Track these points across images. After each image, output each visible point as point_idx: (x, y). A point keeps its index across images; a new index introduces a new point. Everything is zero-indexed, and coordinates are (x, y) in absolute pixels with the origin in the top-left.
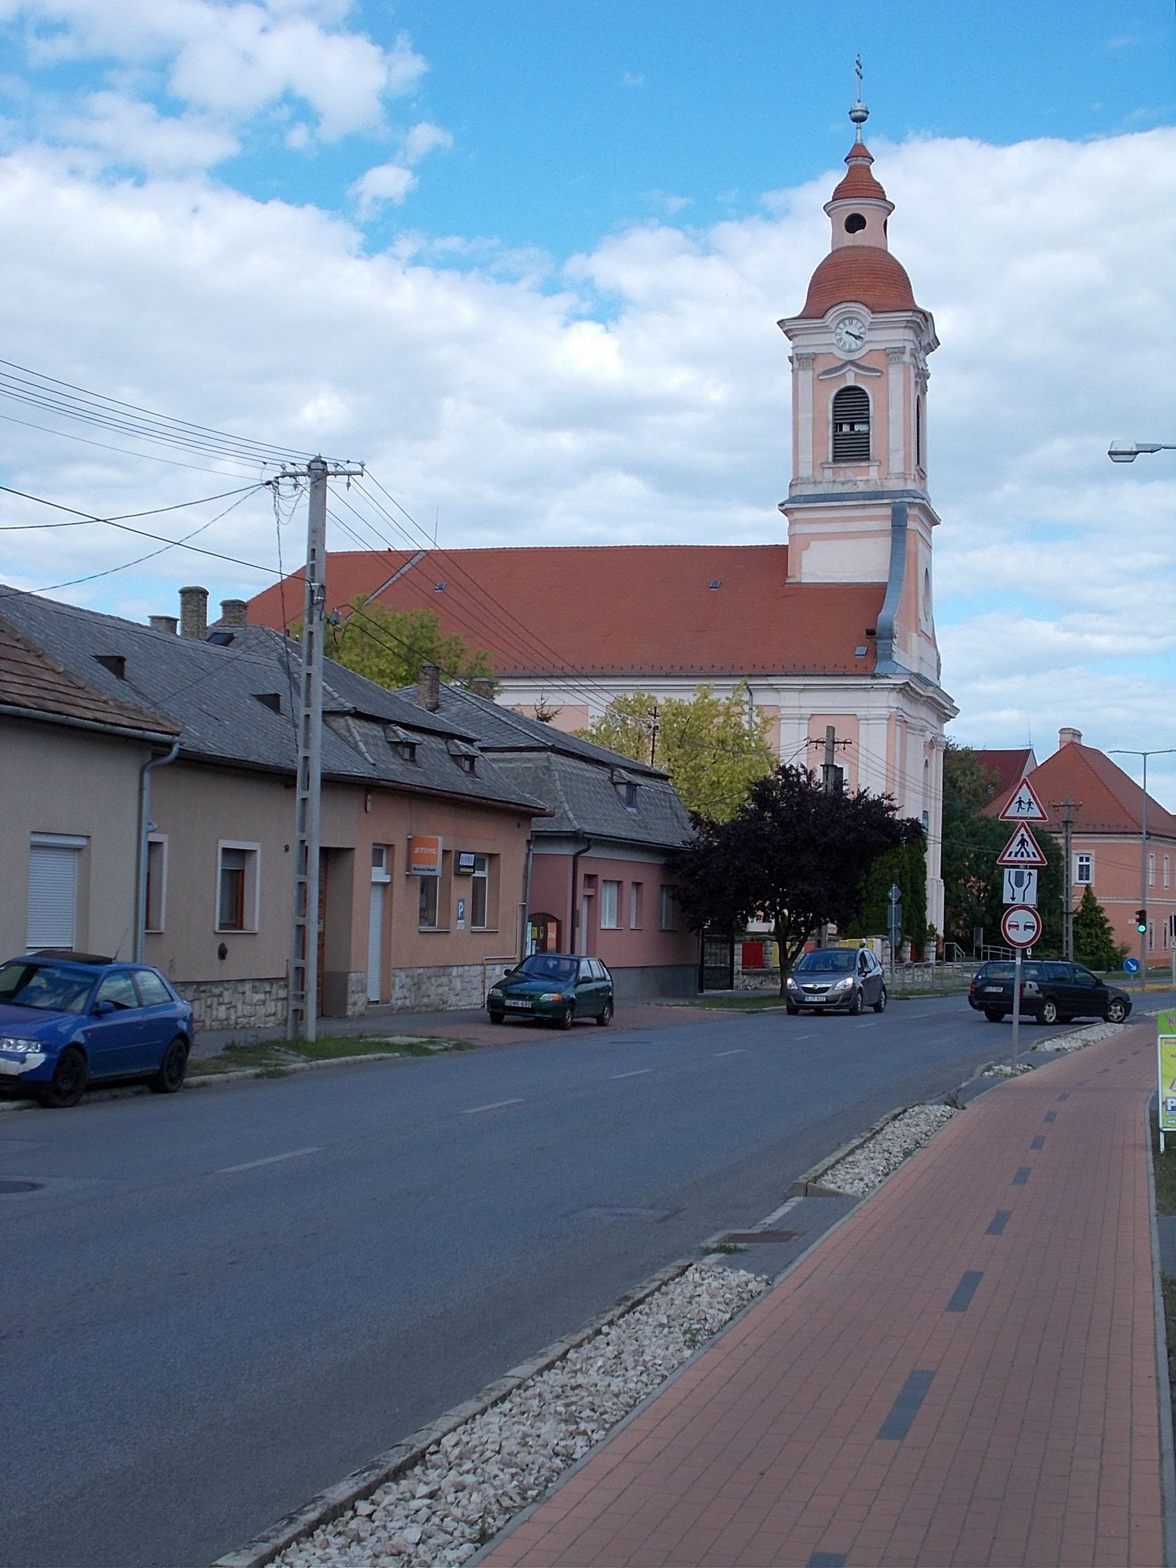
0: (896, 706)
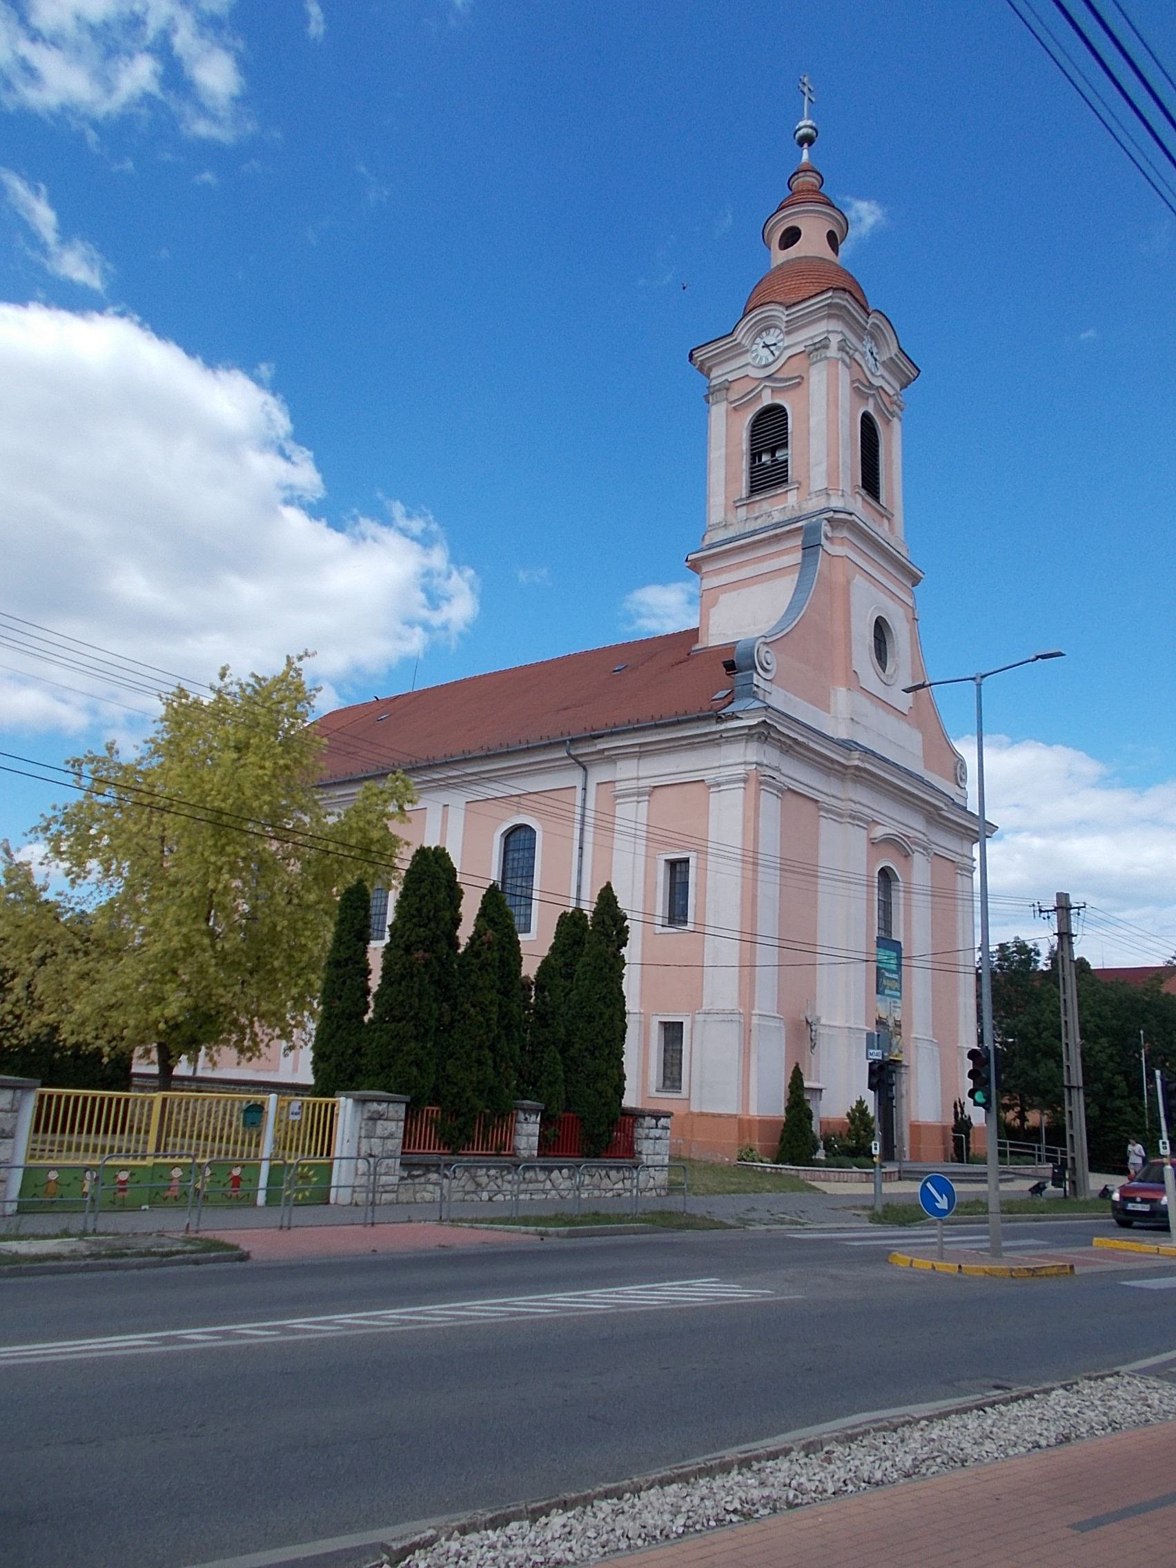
0: (755, 759)
